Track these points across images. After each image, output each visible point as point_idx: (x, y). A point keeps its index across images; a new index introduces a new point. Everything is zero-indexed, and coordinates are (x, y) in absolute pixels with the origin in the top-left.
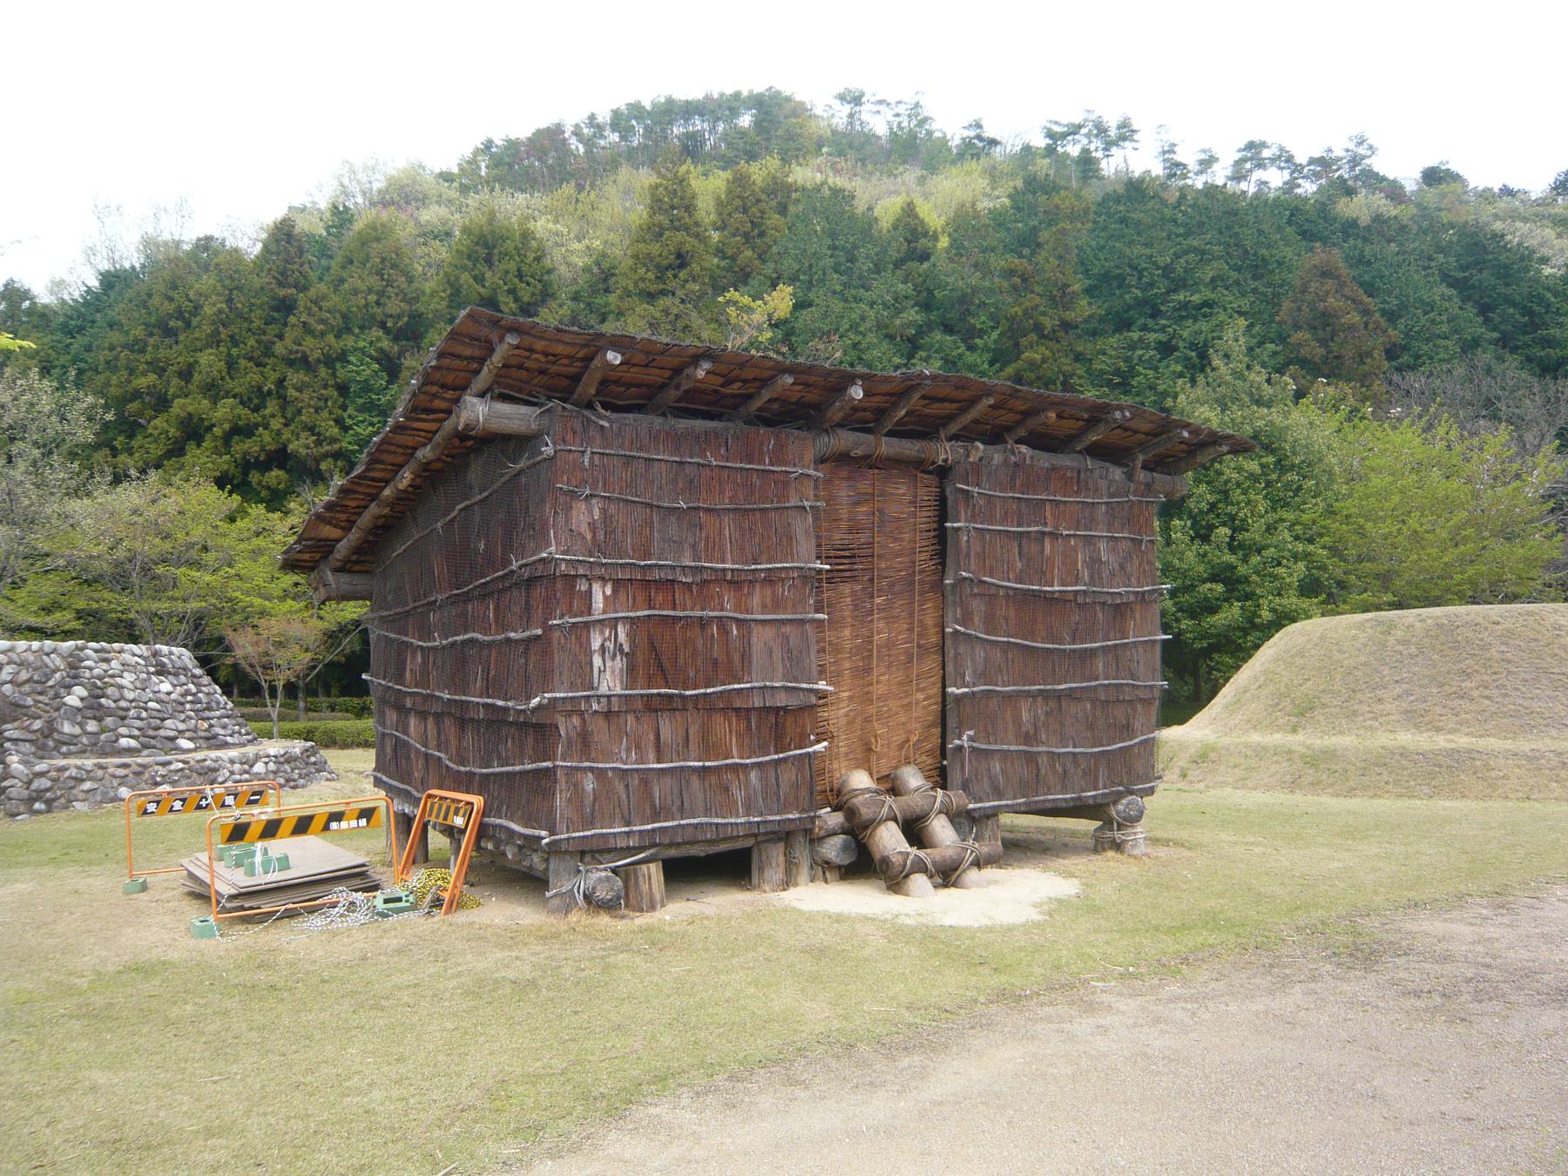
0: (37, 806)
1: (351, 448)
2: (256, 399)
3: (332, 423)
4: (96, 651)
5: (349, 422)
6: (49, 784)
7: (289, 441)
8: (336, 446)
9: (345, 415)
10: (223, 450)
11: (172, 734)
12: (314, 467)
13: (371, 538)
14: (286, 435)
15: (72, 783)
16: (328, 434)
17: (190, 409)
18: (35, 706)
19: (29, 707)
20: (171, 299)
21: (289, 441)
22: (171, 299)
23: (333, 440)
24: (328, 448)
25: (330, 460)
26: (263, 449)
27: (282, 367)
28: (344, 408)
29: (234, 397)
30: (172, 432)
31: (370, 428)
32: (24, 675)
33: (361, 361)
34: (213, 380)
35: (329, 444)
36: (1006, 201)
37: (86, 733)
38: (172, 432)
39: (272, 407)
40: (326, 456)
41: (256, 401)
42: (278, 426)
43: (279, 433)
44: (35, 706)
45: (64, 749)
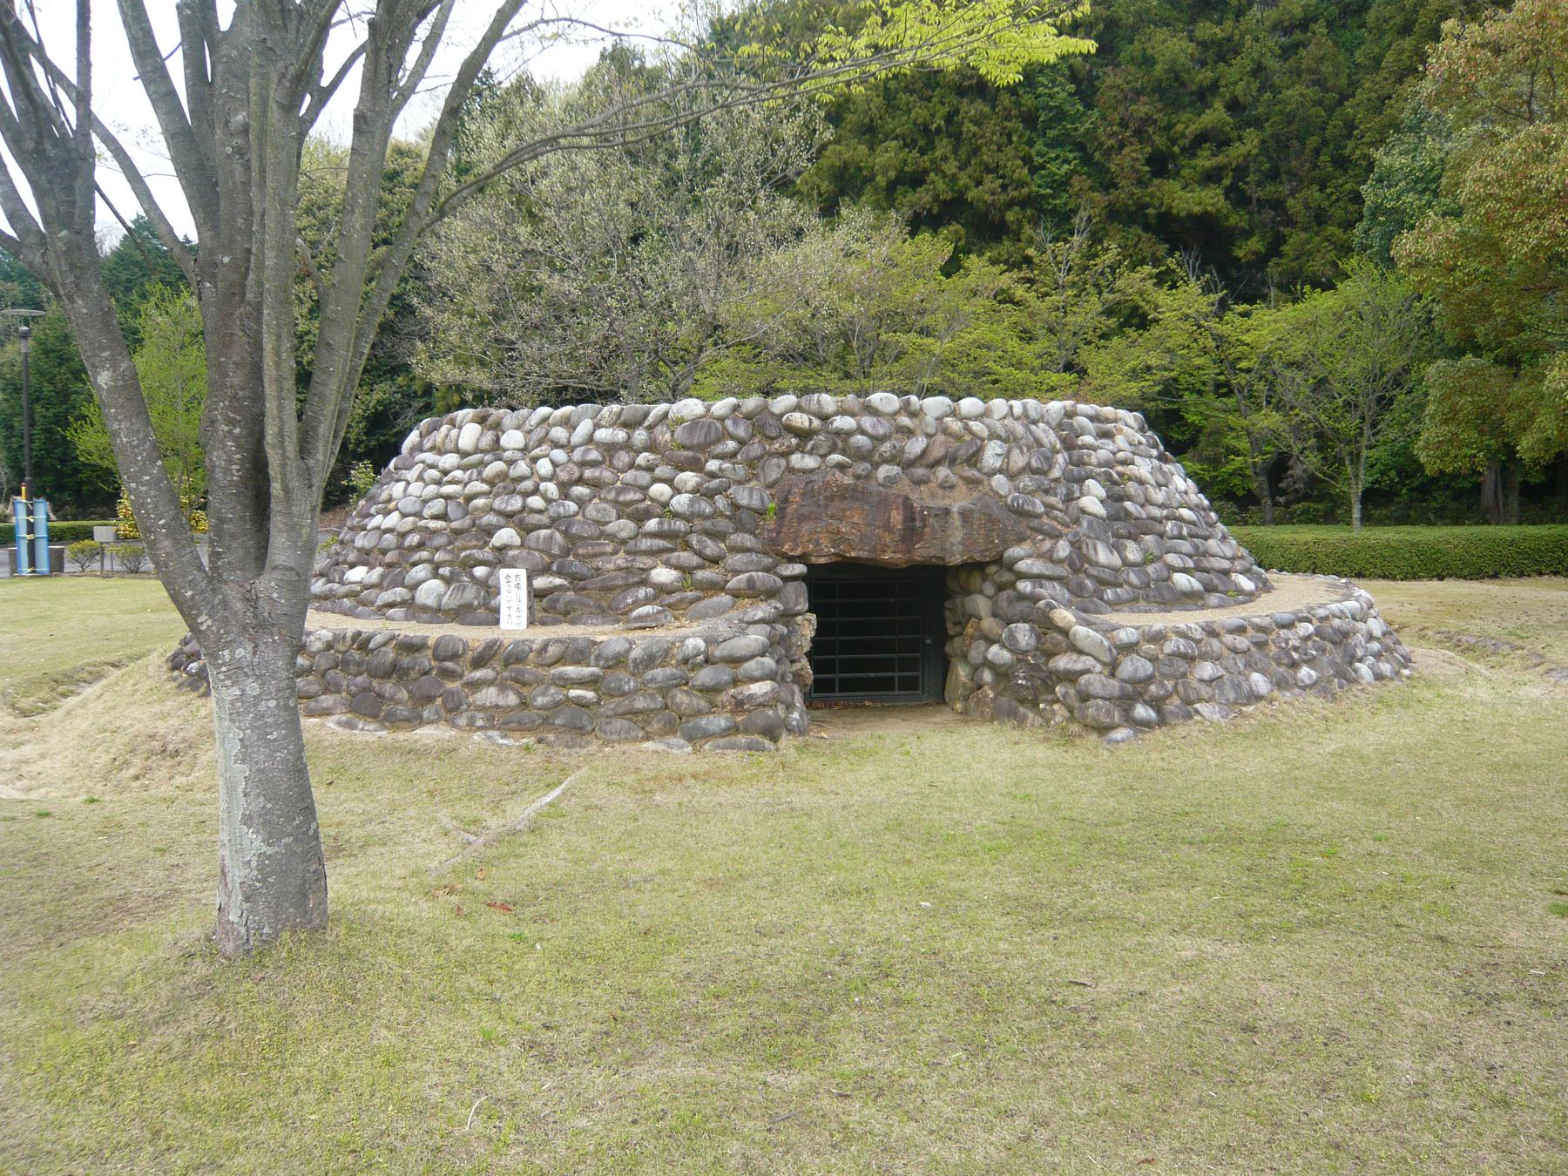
0: (1142, 711)
1: (1042, 191)
2: (923, 137)
3: (1019, 162)
4: (1092, 419)
5: (1038, 160)
6: (1149, 668)
7: (967, 188)
8: (1025, 191)
9: (1033, 152)
10: (884, 205)
11: (1226, 564)
12: (997, 218)
13: (486, 402)
14: (964, 179)
15: (1182, 666)
16: (1015, 176)
17: (846, 156)
18: (1047, 513)
19: (1038, 516)
20: (186, 445)
21: (967, 188)
22: (186, 445)
23: (1021, 184)
24: (1015, 193)
25: (1017, 209)
26: (936, 198)
27: (954, 99)
28: (1031, 143)
29: (896, 138)
30: (825, 186)
31: (1066, 167)
32: (1018, 460)
33: (1053, 82)
34: (871, 120)
35: (1015, 189)
36: (844, 212)
37: (1126, 563)
38: (825, 186)
39: (943, 147)
40: (1010, 204)
41: (921, 143)
42: (954, 170)
43: (954, 179)
44: (1047, 513)
45: (1109, 594)
